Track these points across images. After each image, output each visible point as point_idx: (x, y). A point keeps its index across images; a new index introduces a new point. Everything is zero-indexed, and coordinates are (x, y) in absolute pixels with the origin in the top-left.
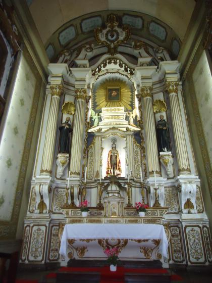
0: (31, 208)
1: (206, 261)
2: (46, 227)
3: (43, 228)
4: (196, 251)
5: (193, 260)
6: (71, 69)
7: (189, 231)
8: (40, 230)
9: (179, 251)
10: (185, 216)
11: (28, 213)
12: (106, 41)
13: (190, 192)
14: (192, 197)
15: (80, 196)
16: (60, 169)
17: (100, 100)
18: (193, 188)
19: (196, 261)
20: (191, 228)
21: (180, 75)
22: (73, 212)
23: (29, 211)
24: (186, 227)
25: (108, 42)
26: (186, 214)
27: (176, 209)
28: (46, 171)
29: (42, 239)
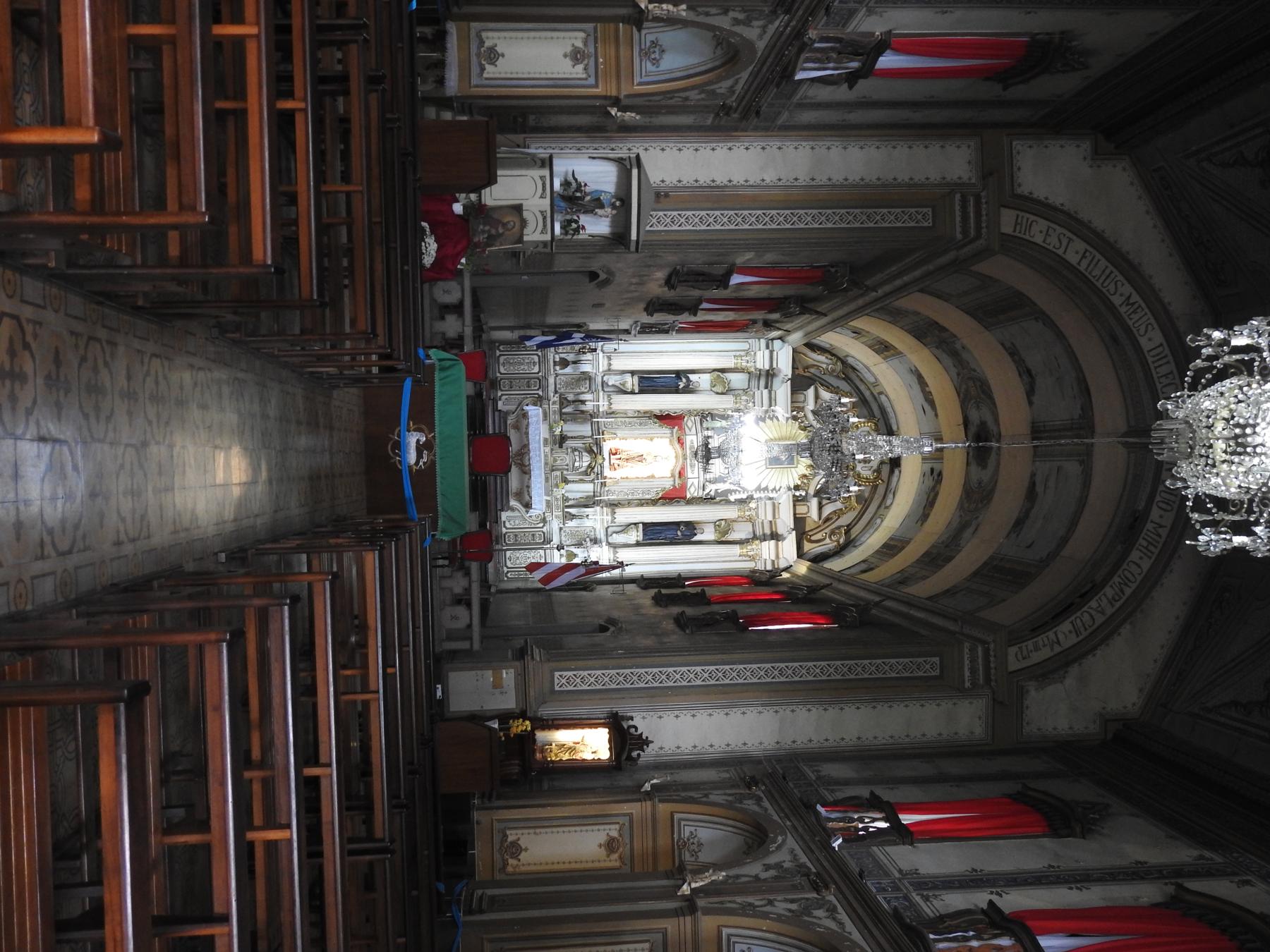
3: (536, 369)
5: (508, 553)
16: (613, 380)
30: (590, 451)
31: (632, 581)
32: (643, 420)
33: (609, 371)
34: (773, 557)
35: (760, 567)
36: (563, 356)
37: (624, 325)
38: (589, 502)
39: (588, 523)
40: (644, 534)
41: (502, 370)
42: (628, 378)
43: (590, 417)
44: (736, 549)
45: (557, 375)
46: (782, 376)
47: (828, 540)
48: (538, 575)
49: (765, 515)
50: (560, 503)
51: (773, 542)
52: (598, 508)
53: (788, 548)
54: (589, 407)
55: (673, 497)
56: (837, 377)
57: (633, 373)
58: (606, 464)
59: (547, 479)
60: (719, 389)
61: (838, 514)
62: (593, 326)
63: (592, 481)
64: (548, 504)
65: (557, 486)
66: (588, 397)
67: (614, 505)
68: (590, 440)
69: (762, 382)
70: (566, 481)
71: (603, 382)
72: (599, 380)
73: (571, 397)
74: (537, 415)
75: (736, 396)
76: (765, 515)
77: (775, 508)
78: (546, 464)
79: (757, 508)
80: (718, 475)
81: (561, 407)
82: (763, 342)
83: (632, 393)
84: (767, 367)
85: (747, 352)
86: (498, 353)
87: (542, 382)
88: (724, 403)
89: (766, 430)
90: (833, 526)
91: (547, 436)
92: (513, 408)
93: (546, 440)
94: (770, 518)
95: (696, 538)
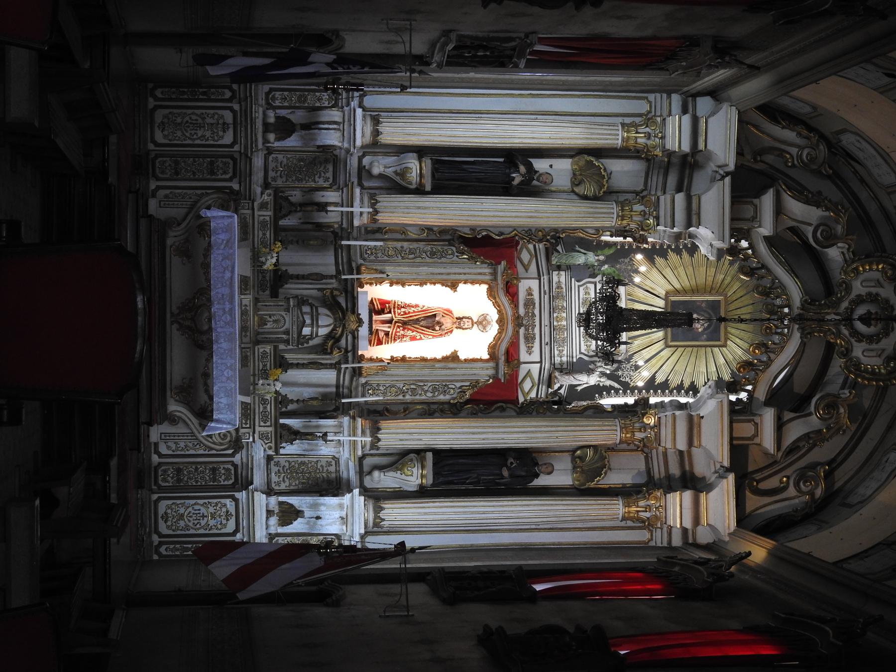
0: (278, 94)
1: (161, 536)
2: (234, 534)
3: (228, 139)
4: (181, 516)
5: (163, 506)
6: (728, 180)
7: (225, 505)
8: (224, 132)
9: (179, 480)
10: (261, 500)
11: (266, 88)
12: (853, 296)
13: (318, 518)
14: (308, 523)
15: (310, 226)
16: (380, 165)
17: (673, 269)
18: (330, 524)
19: (160, 516)
20: (232, 510)
21: (708, 544)
22: (268, 218)
23: (271, 90)
24: (236, 501)
25: (845, 305)
26: (267, 505)
27: (278, 484)
28: (376, 133)
29: (203, 136)
30: (333, 306)
31: (419, 576)
32: (438, 247)
33: (375, 146)
34: (688, 524)
35: (660, 539)
36: (283, 113)
37: (419, 47)
38: (329, 405)
39: (326, 450)
40: (436, 474)
41: (159, 137)
42: (413, 164)
43: (333, 237)
44: (618, 508)
45: (270, 151)
46: (712, 166)
47: (792, 491)
48: (222, 569)
49: (674, 438)
50: (271, 408)
51: (688, 495)
52: (346, 420)
53: (720, 508)
54: (333, 216)
55: (492, 395)
56: (818, 173)
57: (421, 151)
58: (364, 331)
59: (244, 361)
60: (588, 189)
61: (812, 439)
62: (358, 43)
63: (336, 366)
64: (247, 411)
65: (265, 375)
66: (332, 196)
67: (376, 415)
68: (334, 284)
69: (672, 180)
70: (283, 365)
71: (361, 168)
72: (354, 162)
73: (296, 196)
74: (228, 229)
75: (622, 205)
76: (674, 438)
77: (693, 425)
78: (244, 329)
79: (658, 425)
80: (576, 356)
81: (276, 218)
82: (676, 99)
83: (419, 191)
84: (686, 147)
85: (648, 119)
86: (151, 103)
87: (239, 165)
88: (599, 218)
89: (668, 272)
90: (802, 463)
91: (248, 273)
92: (176, 212)
93: (244, 280)
94: (682, 445)
95: (543, 480)
